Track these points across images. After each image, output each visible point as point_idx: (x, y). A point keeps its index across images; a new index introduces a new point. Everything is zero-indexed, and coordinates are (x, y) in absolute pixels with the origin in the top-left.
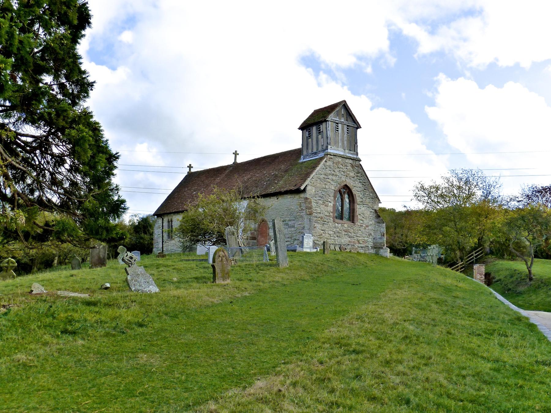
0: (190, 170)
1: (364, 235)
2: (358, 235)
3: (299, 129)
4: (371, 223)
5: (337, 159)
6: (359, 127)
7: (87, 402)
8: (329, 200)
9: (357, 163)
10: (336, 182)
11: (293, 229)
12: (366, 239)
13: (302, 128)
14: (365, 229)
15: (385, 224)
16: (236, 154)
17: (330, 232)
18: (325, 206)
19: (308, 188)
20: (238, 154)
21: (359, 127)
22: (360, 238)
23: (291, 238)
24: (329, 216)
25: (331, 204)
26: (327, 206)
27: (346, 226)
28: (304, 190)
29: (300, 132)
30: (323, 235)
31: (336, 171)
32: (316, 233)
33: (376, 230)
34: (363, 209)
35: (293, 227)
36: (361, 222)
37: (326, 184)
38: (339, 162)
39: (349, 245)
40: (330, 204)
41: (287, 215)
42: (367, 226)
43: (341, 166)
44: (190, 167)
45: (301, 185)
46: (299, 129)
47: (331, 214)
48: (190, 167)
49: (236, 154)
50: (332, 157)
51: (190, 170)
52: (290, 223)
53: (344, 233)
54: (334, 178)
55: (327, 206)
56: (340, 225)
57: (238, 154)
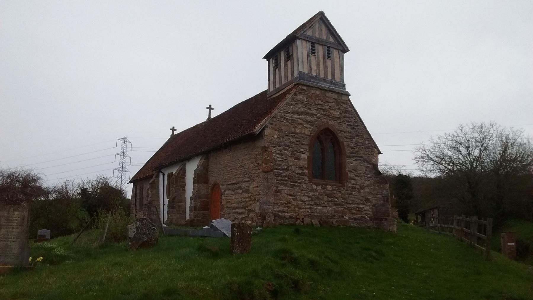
0: (173, 132)
1: (358, 201)
2: (348, 201)
3: (265, 58)
4: (367, 183)
5: (313, 92)
6: (345, 49)
7: (356, 205)
8: (302, 150)
9: (344, 98)
10: (312, 124)
11: (247, 195)
12: (361, 206)
13: (268, 57)
14: (359, 191)
15: (388, 185)
16: (210, 108)
17: (303, 198)
18: (296, 158)
19: (267, 132)
20: (213, 109)
21: (345, 49)
22: (352, 206)
23: (244, 208)
24: (303, 174)
25: (305, 156)
26: (298, 159)
27: (329, 187)
28: (261, 134)
29: (266, 62)
30: (293, 202)
31: (312, 108)
32: (280, 200)
33: (375, 192)
34: (355, 163)
35: (247, 191)
36: (354, 182)
37: (295, 127)
38: (317, 96)
39: (335, 216)
40: (303, 156)
41: (240, 174)
42: (363, 188)
43: (320, 102)
44: (173, 129)
45: (254, 125)
46: (265, 58)
47: (306, 171)
48: (173, 129)
49: (210, 108)
50: (305, 88)
51: (173, 132)
52: (243, 185)
53: (326, 198)
54: (309, 118)
55: (298, 159)
56: (319, 187)
57: (213, 109)
